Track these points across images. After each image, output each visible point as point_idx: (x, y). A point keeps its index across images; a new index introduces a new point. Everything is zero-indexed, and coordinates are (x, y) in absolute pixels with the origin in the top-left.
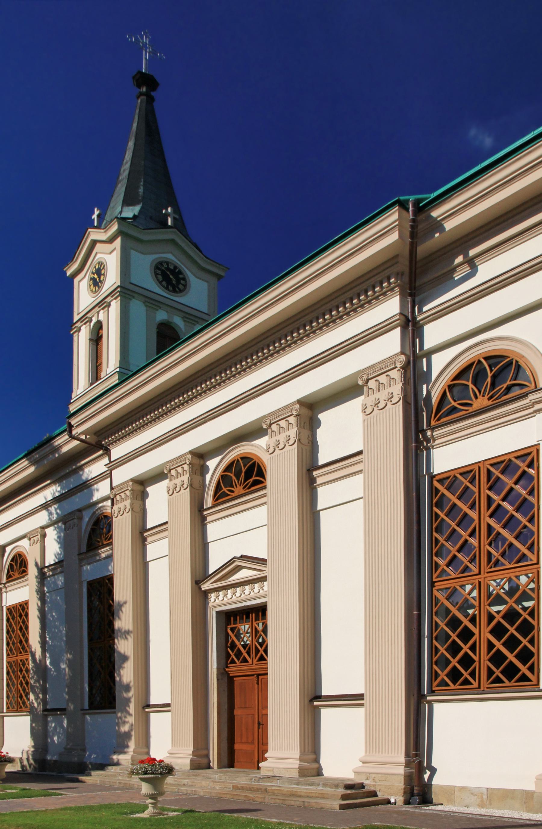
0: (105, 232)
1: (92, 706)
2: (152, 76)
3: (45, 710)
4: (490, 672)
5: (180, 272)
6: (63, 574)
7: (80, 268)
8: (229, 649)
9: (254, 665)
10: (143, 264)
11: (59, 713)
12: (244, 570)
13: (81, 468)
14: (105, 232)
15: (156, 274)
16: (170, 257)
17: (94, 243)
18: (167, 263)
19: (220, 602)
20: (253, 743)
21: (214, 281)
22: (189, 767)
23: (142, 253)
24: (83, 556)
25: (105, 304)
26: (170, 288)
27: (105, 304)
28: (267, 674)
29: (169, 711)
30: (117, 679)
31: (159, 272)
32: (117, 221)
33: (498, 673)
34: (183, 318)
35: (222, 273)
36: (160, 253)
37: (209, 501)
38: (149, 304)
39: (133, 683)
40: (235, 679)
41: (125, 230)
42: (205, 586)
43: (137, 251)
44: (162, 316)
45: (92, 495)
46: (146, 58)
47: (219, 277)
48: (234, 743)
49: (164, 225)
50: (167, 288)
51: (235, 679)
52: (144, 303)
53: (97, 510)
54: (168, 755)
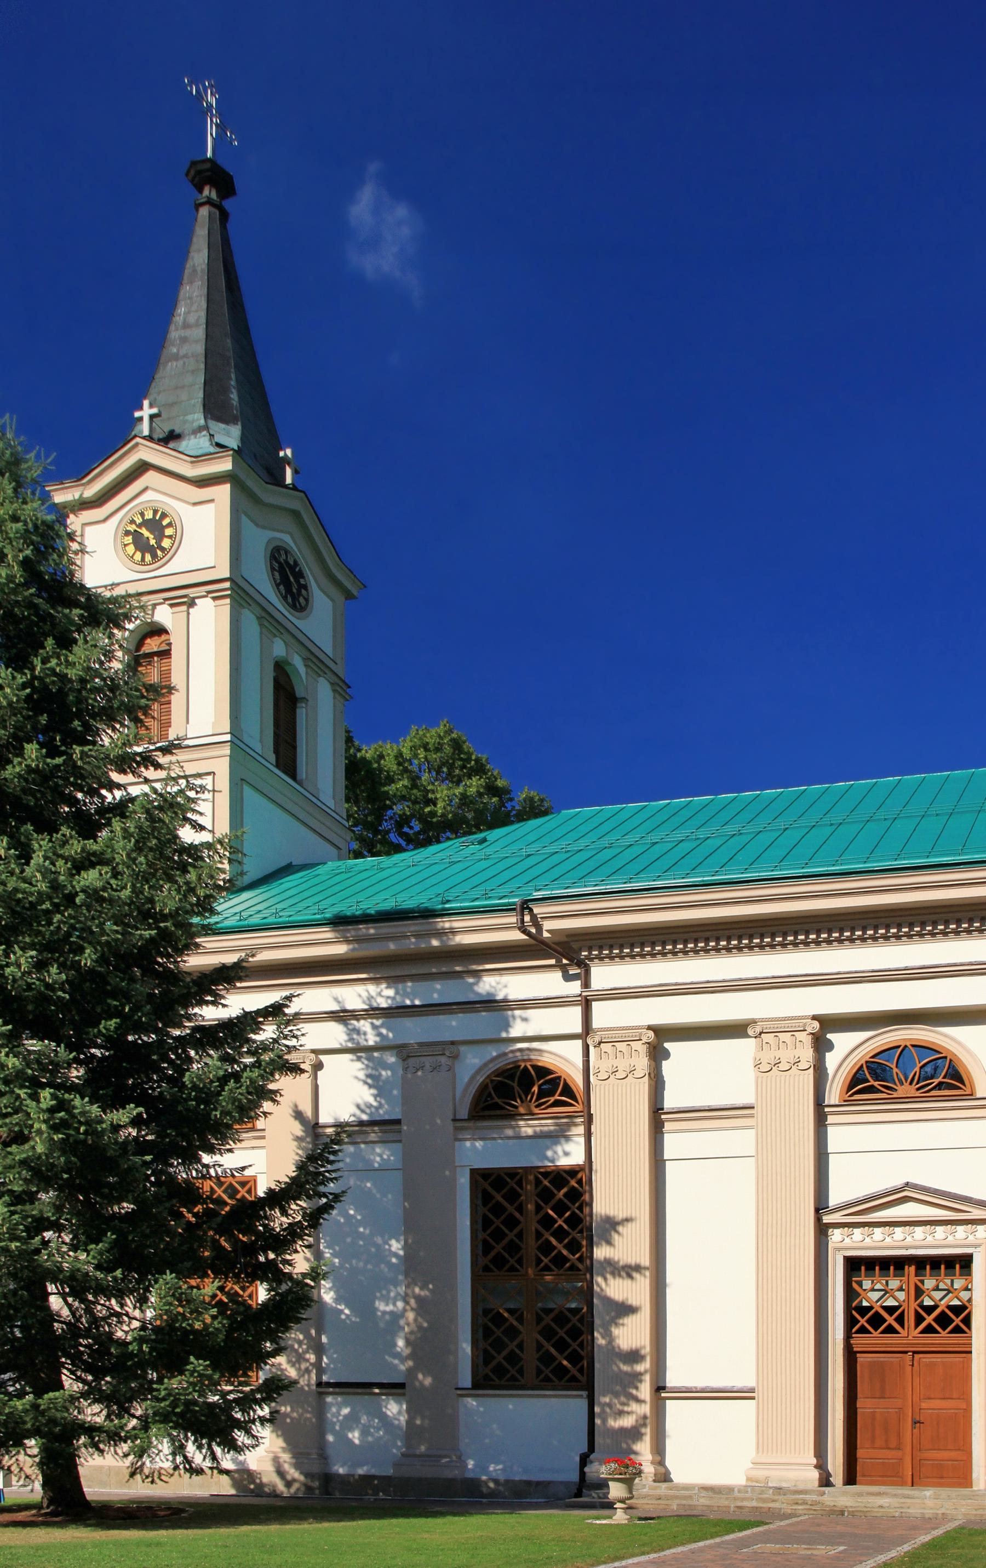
0: (192, 462)
1: (476, 1385)
2: (231, 178)
3: (319, 1384)
4: (539, 1372)
5: (300, 575)
6: (399, 1145)
7: (94, 499)
8: (854, 1312)
9: (910, 1338)
10: (259, 541)
11: (377, 1391)
12: (911, 1205)
13: (477, 974)
14: (192, 462)
15: (273, 569)
16: (287, 538)
17: (143, 468)
18: (286, 552)
19: (846, 1242)
20: (899, 1447)
21: (340, 599)
22: (817, 1483)
23: (257, 525)
24: (459, 1124)
25: (185, 600)
26: (290, 599)
27: (185, 600)
28: (971, 1352)
29: (753, 1398)
30: (600, 1341)
31: (276, 565)
32: (233, 456)
33: (547, 1372)
34: (305, 660)
35: (355, 592)
36: (278, 531)
37: (833, 1095)
38: (266, 624)
39: (648, 1349)
40: (858, 1355)
41: (242, 476)
42: (827, 1219)
43: (252, 521)
44: (279, 649)
45: (507, 1026)
46: (211, 135)
47: (349, 596)
48: (856, 1448)
49: (278, 480)
50: (285, 598)
51: (858, 1355)
52: (258, 618)
53: (512, 1052)
54: (752, 1466)
